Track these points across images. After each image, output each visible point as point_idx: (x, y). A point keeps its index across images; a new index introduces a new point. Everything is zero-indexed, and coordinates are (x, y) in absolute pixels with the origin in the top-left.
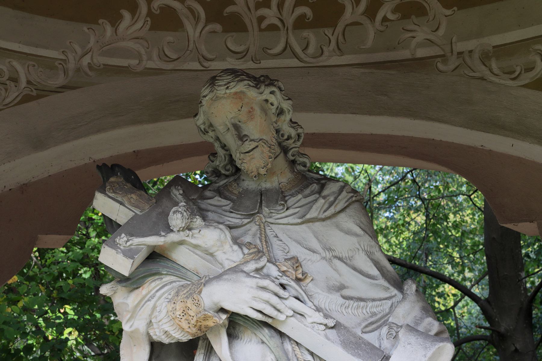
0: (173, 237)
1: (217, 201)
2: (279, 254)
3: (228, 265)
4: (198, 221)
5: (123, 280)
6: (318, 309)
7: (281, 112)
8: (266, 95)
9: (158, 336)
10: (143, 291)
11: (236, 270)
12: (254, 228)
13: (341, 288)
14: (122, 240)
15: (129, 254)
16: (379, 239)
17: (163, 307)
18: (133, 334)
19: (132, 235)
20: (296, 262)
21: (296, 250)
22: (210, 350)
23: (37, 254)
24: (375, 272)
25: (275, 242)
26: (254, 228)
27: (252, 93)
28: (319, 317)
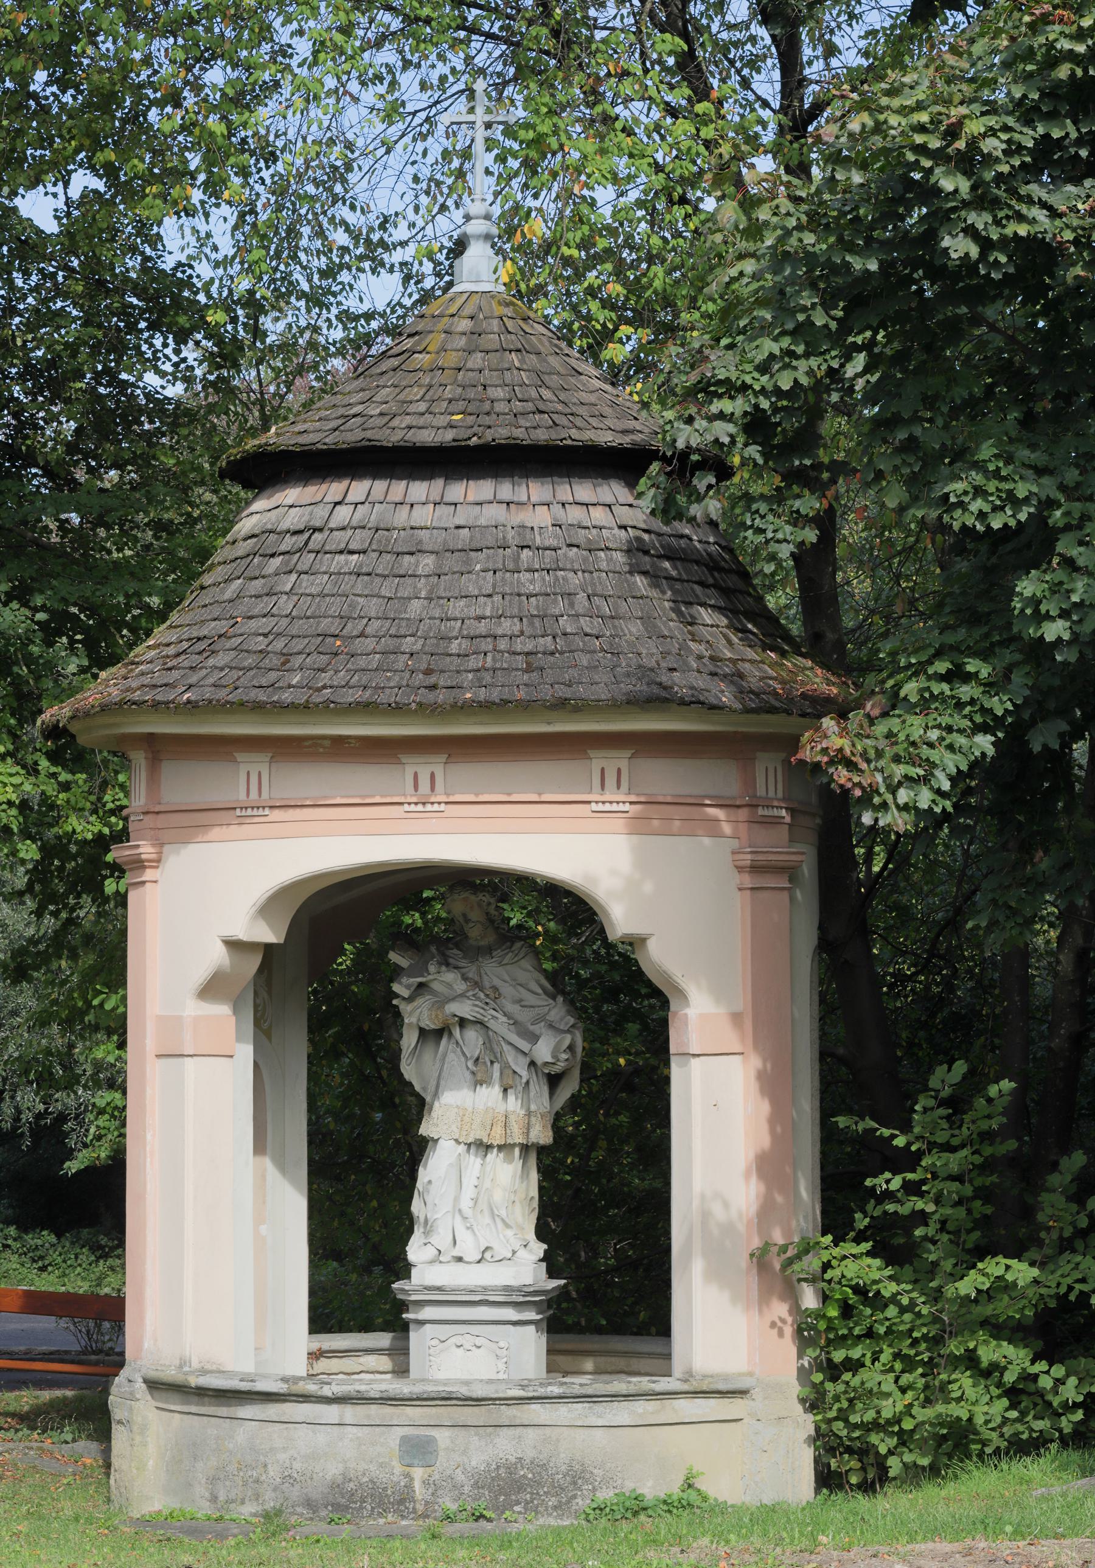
0: (430, 977)
1: (455, 951)
2: (487, 984)
3: (459, 992)
4: (444, 968)
5: (404, 999)
6: (505, 1015)
7: (489, 904)
8: (481, 896)
9: (422, 1025)
10: (415, 1004)
11: (463, 995)
12: (474, 968)
13: (521, 1000)
14: (404, 980)
15: (408, 987)
16: (330, 1262)
17: (426, 1013)
18: (410, 1024)
19: (410, 976)
20: (495, 989)
21: (497, 982)
22: (450, 1034)
23: (63, 331)
24: (540, 991)
25: (485, 977)
26: (474, 968)
27: (473, 897)
28: (505, 1019)
